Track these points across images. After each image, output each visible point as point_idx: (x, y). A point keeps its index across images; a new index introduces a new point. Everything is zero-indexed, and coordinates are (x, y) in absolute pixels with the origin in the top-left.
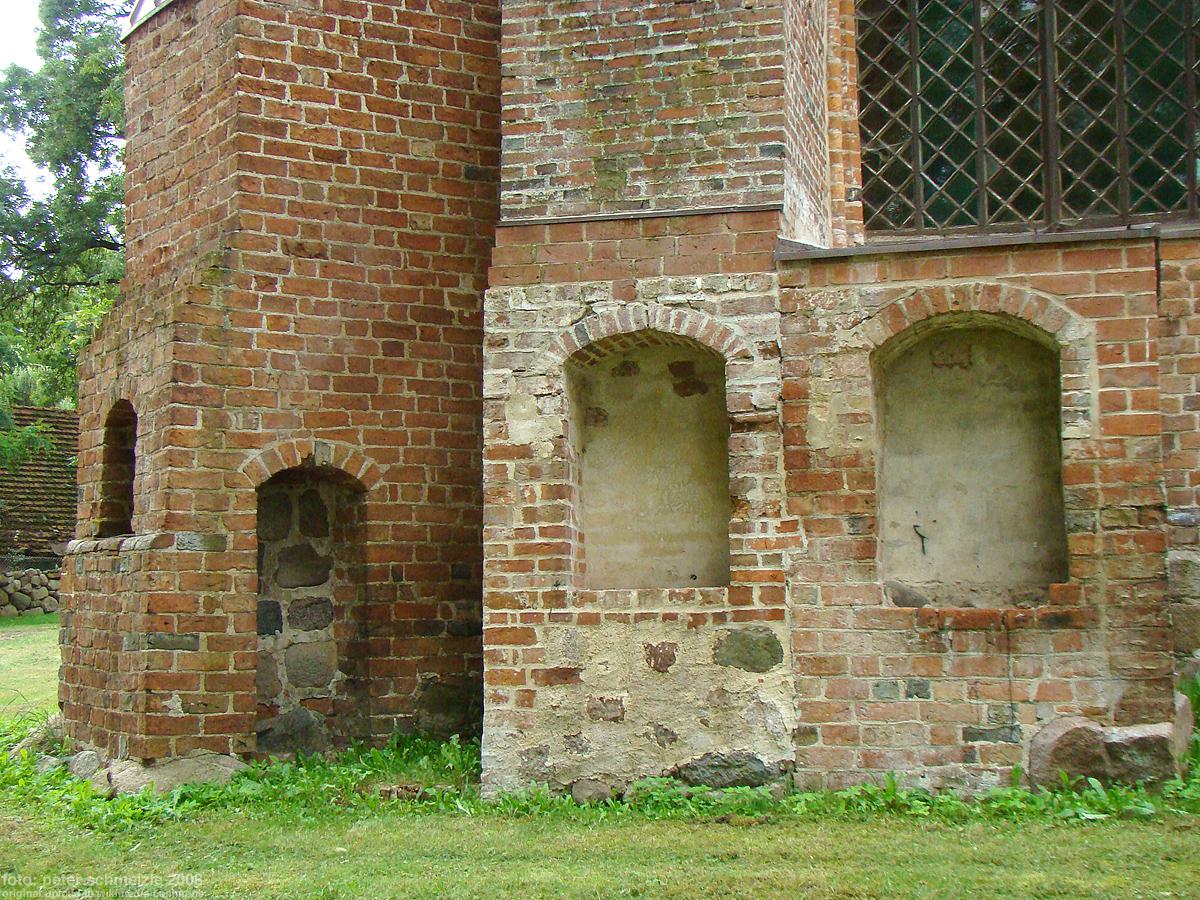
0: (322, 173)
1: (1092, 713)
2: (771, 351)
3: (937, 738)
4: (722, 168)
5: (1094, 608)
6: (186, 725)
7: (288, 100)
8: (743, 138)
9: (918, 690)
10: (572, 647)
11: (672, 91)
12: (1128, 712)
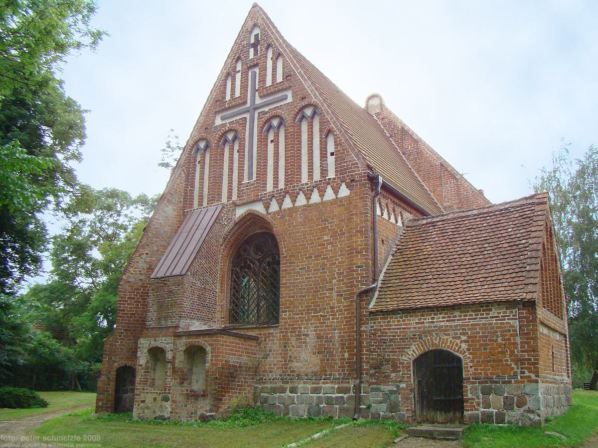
0: (131, 317)
1: (206, 411)
2: (171, 350)
3: (188, 414)
4: (173, 319)
5: (208, 394)
6: (102, 407)
7: (337, 262)
8: (176, 314)
9: (186, 406)
10: (145, 397)
11: (167, 306)
12: (211, 411)
